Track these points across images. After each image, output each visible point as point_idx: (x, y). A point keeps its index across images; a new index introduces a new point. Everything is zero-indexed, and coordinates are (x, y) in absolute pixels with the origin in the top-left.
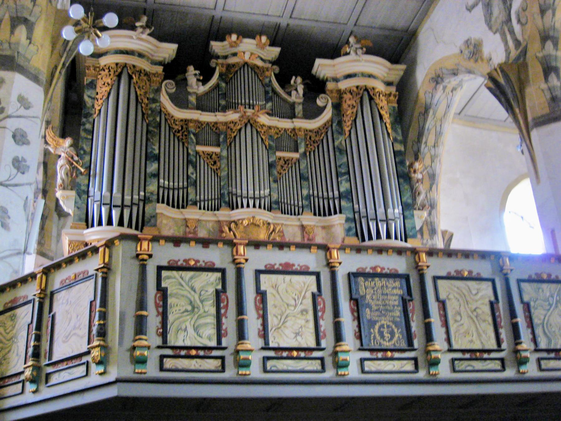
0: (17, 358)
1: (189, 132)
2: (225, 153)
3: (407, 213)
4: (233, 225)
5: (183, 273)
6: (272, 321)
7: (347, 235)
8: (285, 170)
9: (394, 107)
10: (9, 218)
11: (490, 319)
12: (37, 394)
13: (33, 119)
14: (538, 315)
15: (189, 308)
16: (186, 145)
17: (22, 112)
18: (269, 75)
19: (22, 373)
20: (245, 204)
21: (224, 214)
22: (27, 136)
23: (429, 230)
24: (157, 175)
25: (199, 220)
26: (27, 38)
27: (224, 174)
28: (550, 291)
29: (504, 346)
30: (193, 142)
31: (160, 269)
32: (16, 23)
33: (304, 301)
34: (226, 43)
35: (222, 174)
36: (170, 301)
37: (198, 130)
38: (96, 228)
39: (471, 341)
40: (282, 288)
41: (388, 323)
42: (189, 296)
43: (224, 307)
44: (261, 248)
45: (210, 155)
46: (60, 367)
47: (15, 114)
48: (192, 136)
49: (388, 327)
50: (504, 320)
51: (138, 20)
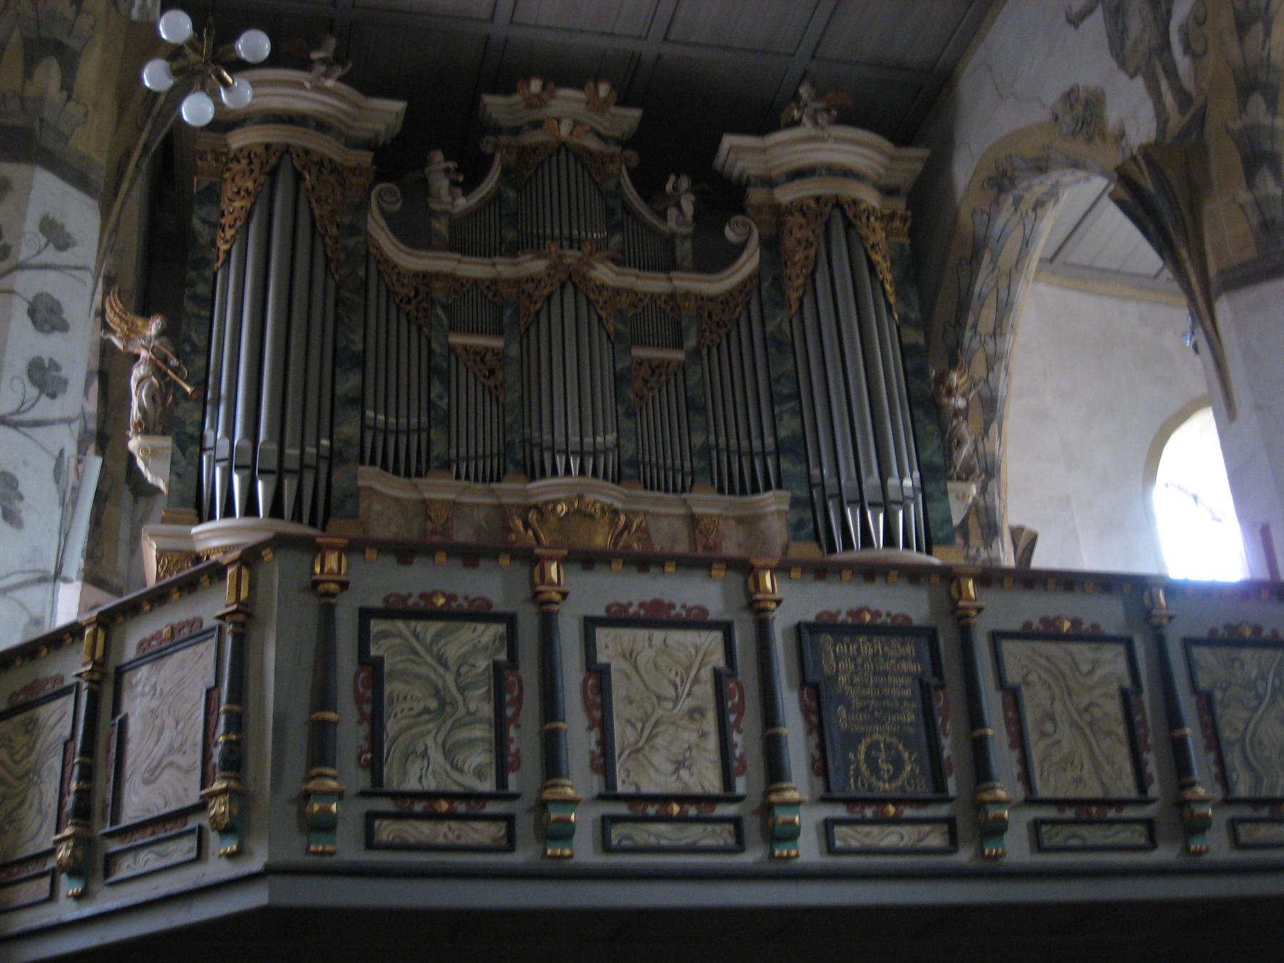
0: (38, 821)
2: (514, 351)
3: (931, 487)
4: (532, 516)
5: (420, 626)
6: (623, 734)
7: (795, 538)
8: (652, 389)
9: (902, 245)
10: (21, 498)
11: (1121, 730)
13: (77, 273)
14: (1232, 720)
15: (433, 704)
16: (426, 330)
17: (51, 255)
19: (52, 852)
21: (512, 490)
24: (359, 401)
25: (454, 504)
26: (62, 88)
27: (512, 397)
29: (1154, 790)
31: (366, 615)
34: (517, 98)
36: (391, 688)
39: (1079, 781)
40: (646, 656)
42: (433, 676)
45: (480, 355)
47: (33, 261)
48: (440, 311)
49: (888, 747)
50: (1153, 736)
51: (317, 46)
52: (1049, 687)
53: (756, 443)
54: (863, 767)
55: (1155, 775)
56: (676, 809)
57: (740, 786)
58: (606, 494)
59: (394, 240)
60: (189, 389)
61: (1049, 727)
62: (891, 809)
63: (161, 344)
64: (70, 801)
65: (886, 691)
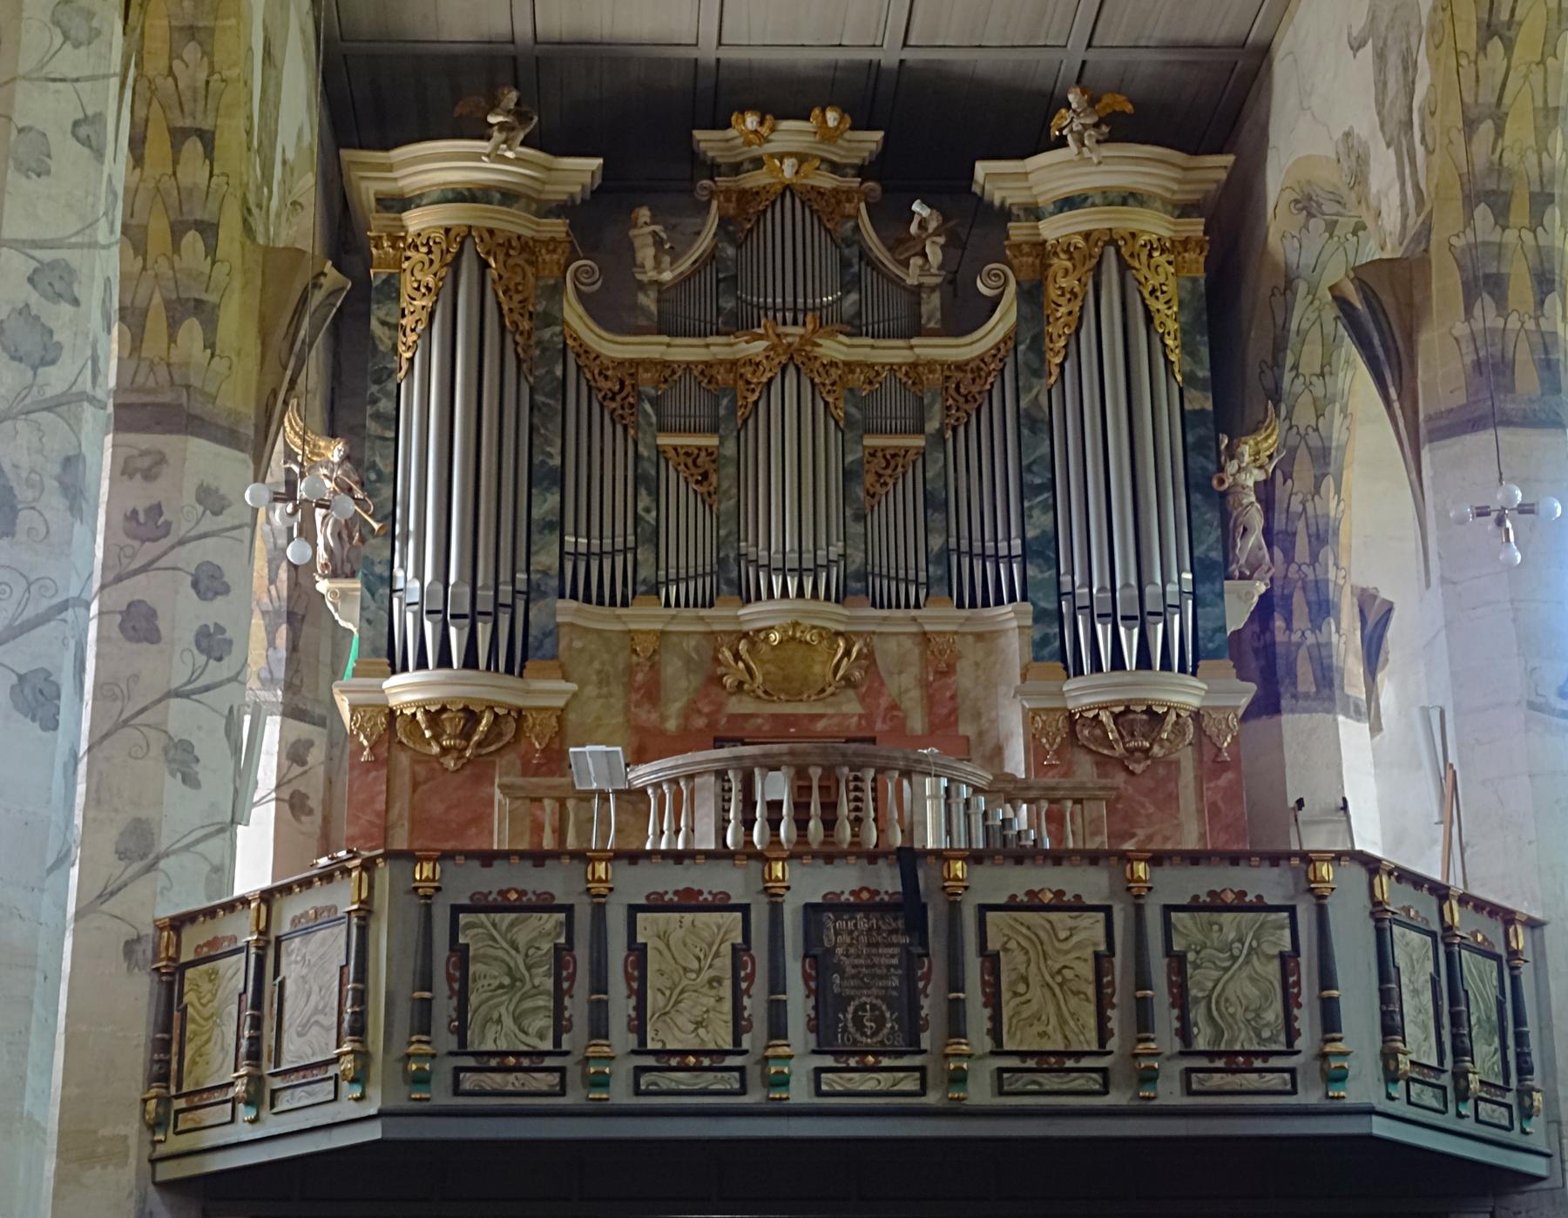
0: (221, 1057)
1: (639, 396)
2: (730, 449)
3: (1203, 590)
4: (743, 646)
5: (497, 917)
7: (1036, 659)
8: (885, 484)
10: (198, 760)
11: (1090, 991)
12: (256, 1126)
13: (234, 533)
14: (1200, 981)
15: (507, 981)
16: (631, 432)
17: (209, 523)
18: (852, 212)
19: (231, 1084)
20: (777, 591)
22: (222, 576)
23: (1309, 604)
25: (663, 633)
28: (1238, 929)
30: (650, 424)
31: (456, 910)
32: (178, 315)
33: (717, 962)
34: (731, 133)
35: (723, 507)
37: (664, 386)
38: (412, 676)
39: (1043, 1035)
41: (879, 1002)
42: (507, 958)
43: (567, 979)
44: (641, 862)
45: (692, 456)
46: (295, 1080)
47: (192, 533)
48: (648, 407)
52: (1027, 953)
53: (1003, 545)
54: (850, 1025)
55: (1116, 1031)
56: (692, 1060)
57: (746, 1042)
58: (834, 616)
59: (597, 329)
60: (376, 526)
61: (1021, 988)
62: (871, 1059)
63: (346, 473)
64: (244, 1043)
65: (876, 960)
